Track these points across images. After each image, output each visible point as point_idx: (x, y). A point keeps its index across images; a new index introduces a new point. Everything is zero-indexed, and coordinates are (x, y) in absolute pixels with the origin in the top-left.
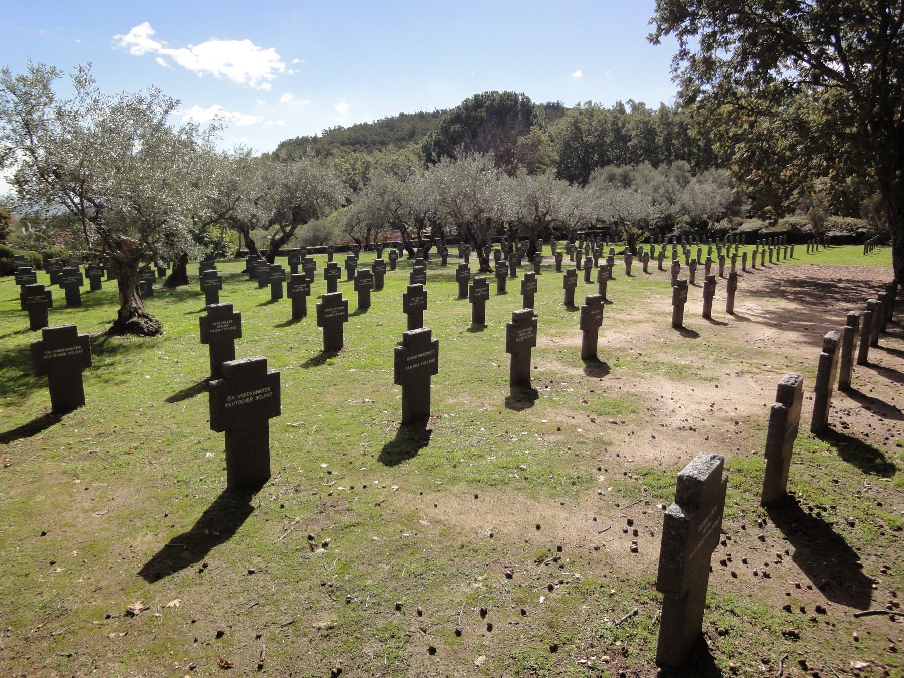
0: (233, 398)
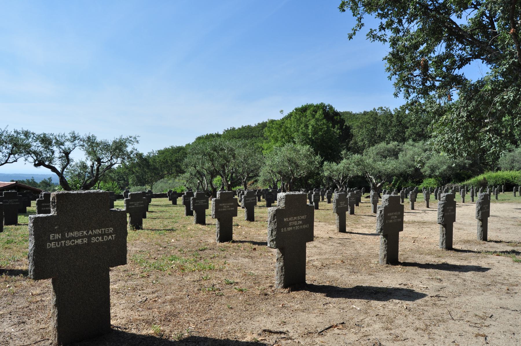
0: (58, 236)
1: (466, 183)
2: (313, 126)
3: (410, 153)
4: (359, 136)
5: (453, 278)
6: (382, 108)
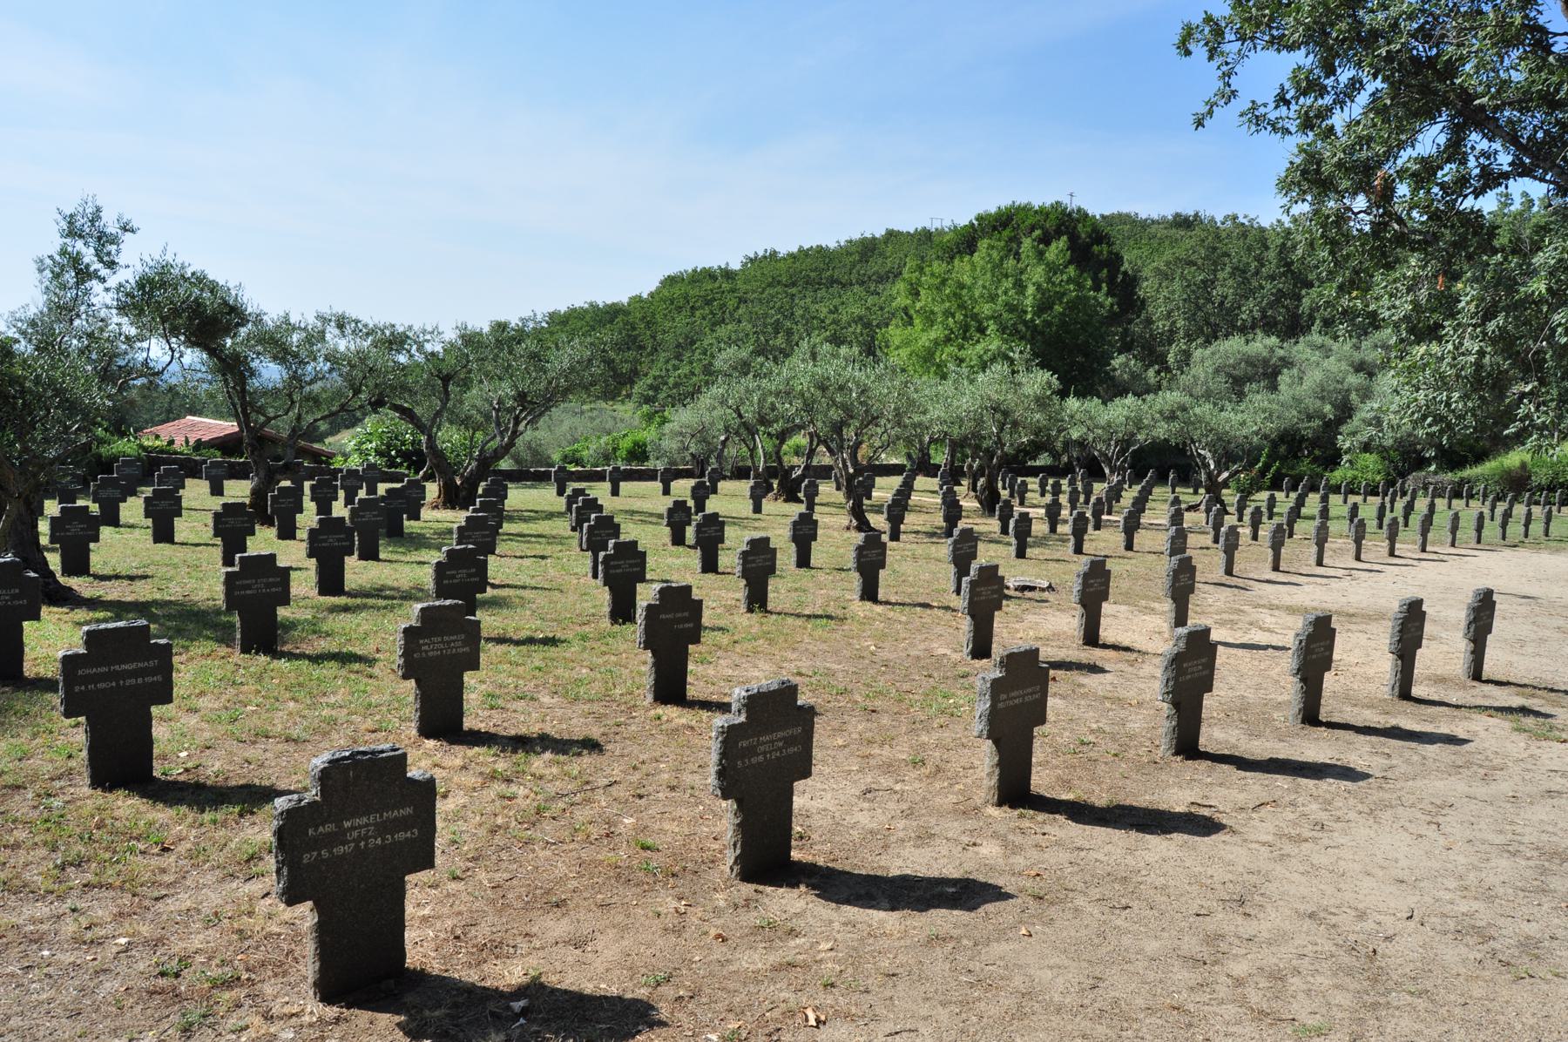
1: (1468, 472)
2: (1039, 287)
3: (1314, 377)
4: (1163, 301)
5: (1407, 754)
6: (1235, 218)
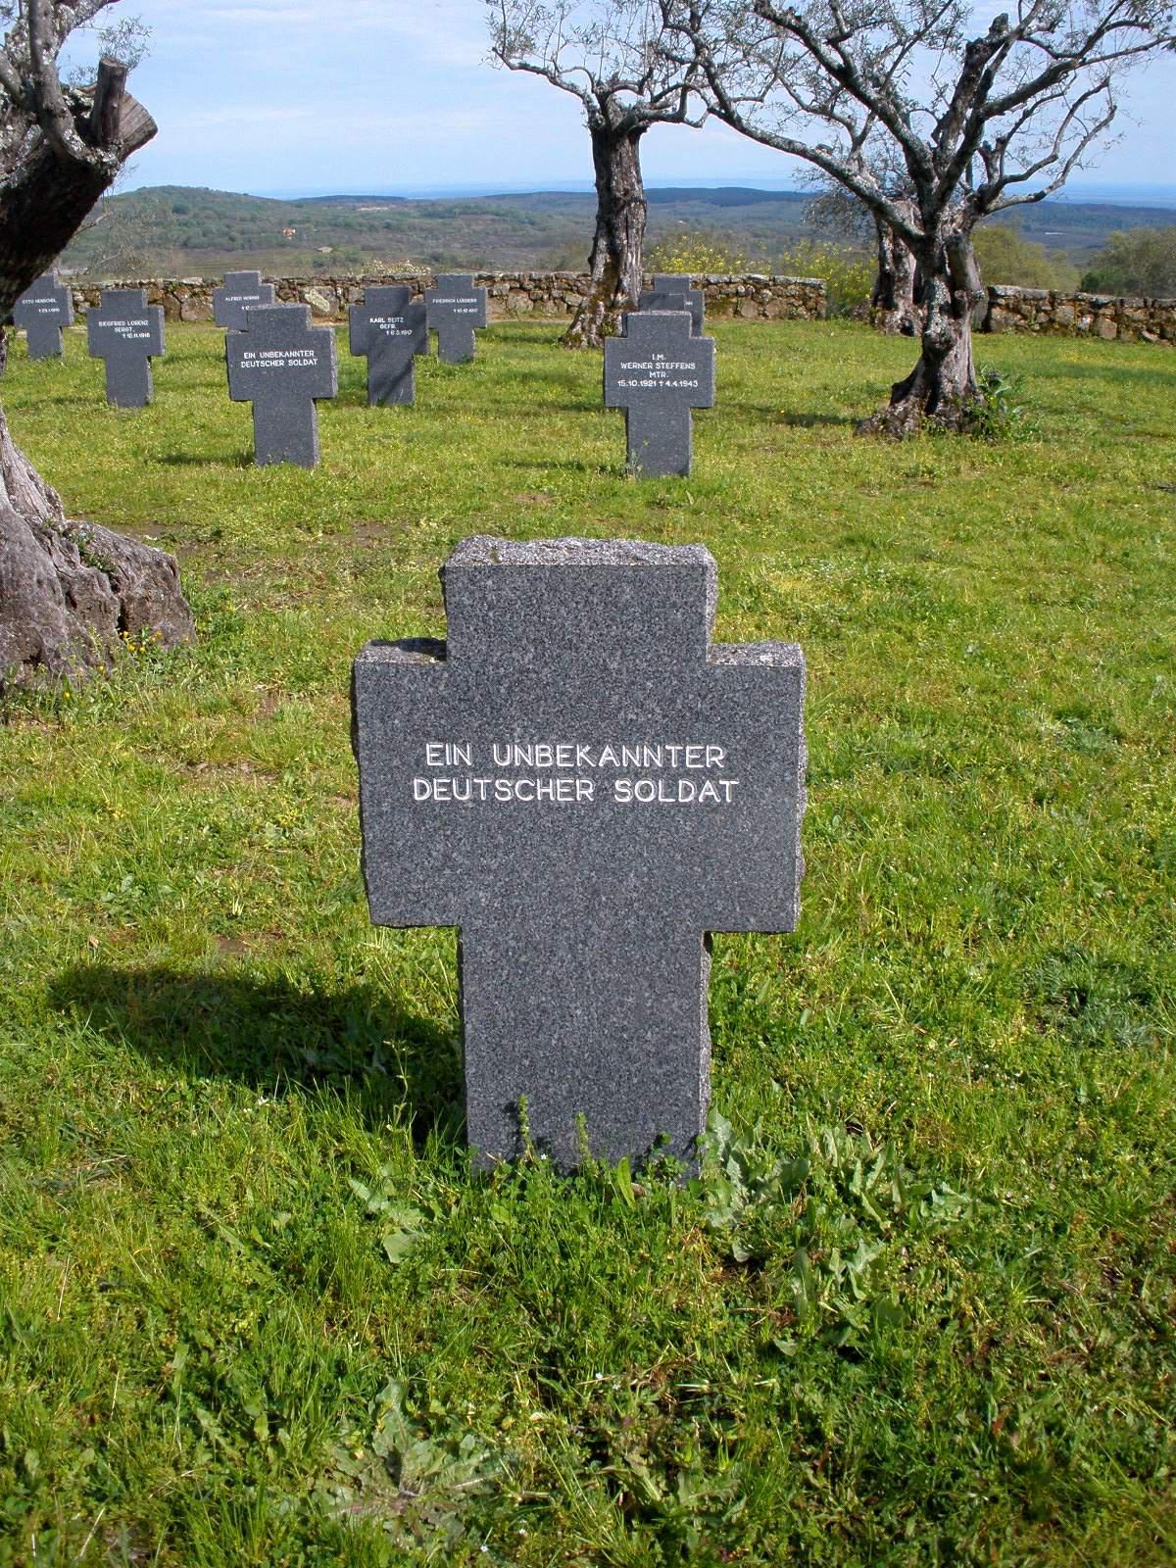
0: (252, 355)
